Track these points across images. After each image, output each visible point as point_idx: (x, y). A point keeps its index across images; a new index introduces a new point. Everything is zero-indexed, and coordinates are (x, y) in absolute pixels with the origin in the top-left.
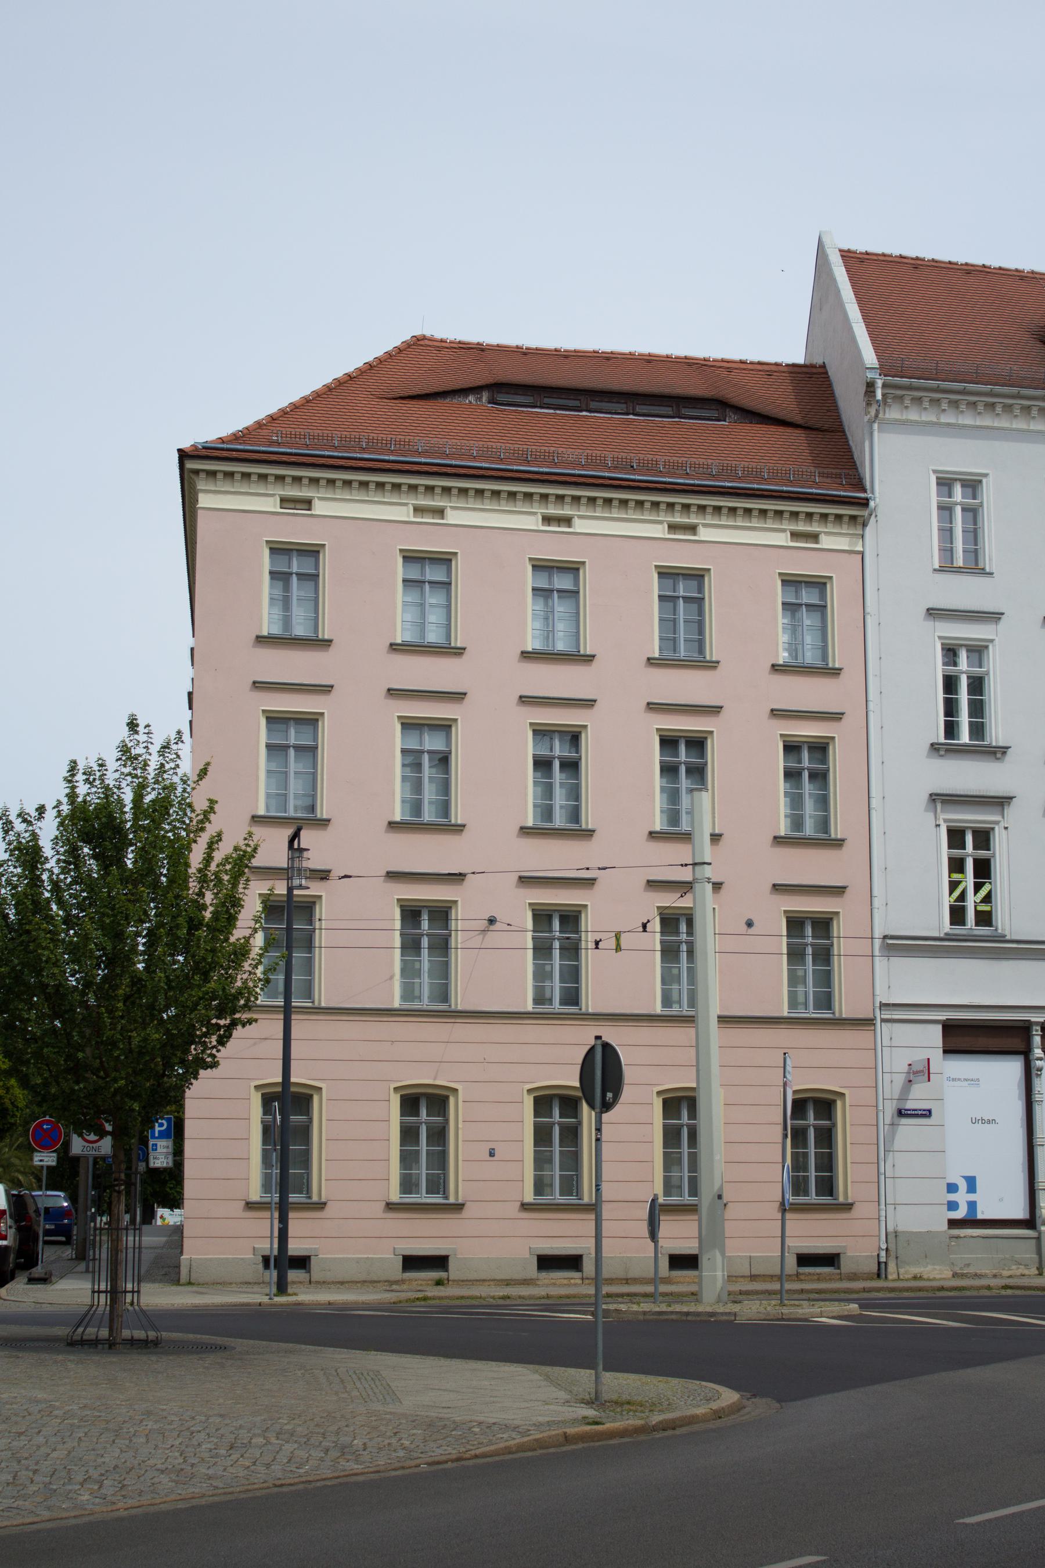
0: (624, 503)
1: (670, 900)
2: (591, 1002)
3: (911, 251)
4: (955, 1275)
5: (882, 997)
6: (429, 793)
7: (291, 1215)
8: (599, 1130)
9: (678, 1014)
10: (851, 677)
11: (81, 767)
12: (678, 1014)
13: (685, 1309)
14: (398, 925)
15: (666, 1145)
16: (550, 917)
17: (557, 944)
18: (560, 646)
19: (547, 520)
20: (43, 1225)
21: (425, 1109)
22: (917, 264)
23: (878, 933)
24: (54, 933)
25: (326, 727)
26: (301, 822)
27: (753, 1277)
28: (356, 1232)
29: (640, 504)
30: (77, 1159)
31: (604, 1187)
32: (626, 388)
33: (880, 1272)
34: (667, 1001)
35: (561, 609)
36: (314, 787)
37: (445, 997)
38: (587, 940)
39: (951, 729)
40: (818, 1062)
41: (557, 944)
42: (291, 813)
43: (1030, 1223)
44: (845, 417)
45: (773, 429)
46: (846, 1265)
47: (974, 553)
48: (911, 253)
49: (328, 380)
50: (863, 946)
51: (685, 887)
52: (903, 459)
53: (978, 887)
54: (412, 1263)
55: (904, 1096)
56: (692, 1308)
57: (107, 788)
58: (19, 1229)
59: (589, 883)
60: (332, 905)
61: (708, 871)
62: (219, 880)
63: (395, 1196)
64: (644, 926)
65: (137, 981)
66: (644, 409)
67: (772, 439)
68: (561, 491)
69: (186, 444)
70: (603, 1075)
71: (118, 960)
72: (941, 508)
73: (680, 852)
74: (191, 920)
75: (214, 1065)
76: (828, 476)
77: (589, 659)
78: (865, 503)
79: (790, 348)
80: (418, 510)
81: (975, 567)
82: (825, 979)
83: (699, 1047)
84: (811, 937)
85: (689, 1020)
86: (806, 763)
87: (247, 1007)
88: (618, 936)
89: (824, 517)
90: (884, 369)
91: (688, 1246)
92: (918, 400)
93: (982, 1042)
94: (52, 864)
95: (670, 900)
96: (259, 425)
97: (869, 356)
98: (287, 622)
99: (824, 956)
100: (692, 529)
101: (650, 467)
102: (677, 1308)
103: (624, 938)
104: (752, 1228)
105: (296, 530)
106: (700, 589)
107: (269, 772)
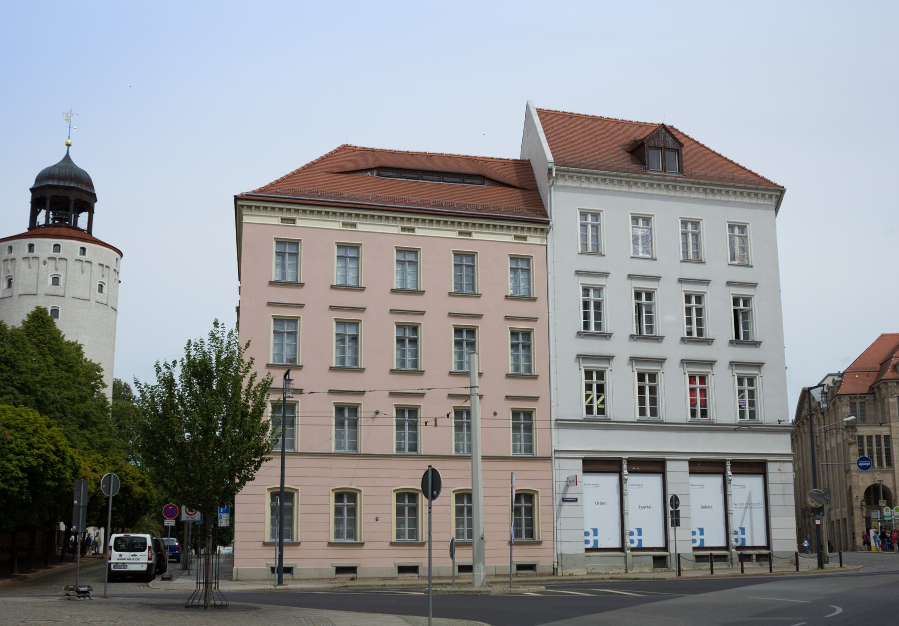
0: (438, 222)
1: (459, 403)
2: (423, 449)
3: (568, 110)
4: (588, 573)
5: (555, 447)
6: (348, 354)
7: (284, 548)
8: (430, 508)
9: (464, 455)
10: (541, 301)
11: (193, 343)
12: (464, 455)
13: (467, 589)
14: (334, 414)
15: (457, 515)
16: (462, 413)
17: (407, 423)
18: (409, 287)
19: (403, 229)
20: (168, 554)
21: (346, 499)
22: (571, 116)
23: (553, 419)
24: (180, 419)
25: (301, 323)
26: (291, 366)
27: (496, 576)
28: (314, 555)
29: (446, 222)
30: (183, 523)
31: (432, 534)
32: (439, 170)
33: (554, 572)
34: (457, 450)
35: (351, 266)
36: (295, 351)
37: (355, 448)
38: (421, 422)
39: (586, 325)
40: (527, 477)
41: (407, 423)
42: (285, 363)
43: (622, 549)
44: (539, 184)
45: (506, 188)
46: (539, 570)
47: (597, 246)
48: (568, 110)
49: (303, 164)
50: (547, 425)
51: (467, 397)
52: (565, 203)
53: (598, 397)
54: (340, 570)
55: (565, 492)
56: (470, 589)
57: (204, 352)
58: (157, 555)
59: (422, 395)
60: (304, 406)
61: (477, 391)
62: (255, 394)
63: (332, 540)
64: (448, 415)
65: (218, 441)
66: (448, 179)
67: (507, 193)
68: (410, 216)
69: (238, 193)
70: (432, 484)
71: (208, 431)
72: (582, 225)
73: (465, 381)
74: (242, 413)
75: (253, 479)
76: (531, 210)
77: (422, 293)
78: (547, 223)
79: (515, 154)
80: (344, 224)
81: (597, 252)
82: (529, 439)
83: (473, 470)
84: (523, 420)
85: (469, 458)
86: (521, 340)
87: (268, 452)
88: (436, 420)
89: (529, 229)
90: (556, 163)
91: (468, 562)
92: (571, 177)
93: (601, 467)
94: (179, 387)
95: (459, 403)
96: (272, 185)
97: (550, 157)
98: (283, 275)
99: (529, 428)
100: (470, 234)
101: (450, 206)
102: (463, 589)
103: (438, 421)
104: (496, 553)
105: (289, 233)
106: (473, 261)
107: (274, 344)
